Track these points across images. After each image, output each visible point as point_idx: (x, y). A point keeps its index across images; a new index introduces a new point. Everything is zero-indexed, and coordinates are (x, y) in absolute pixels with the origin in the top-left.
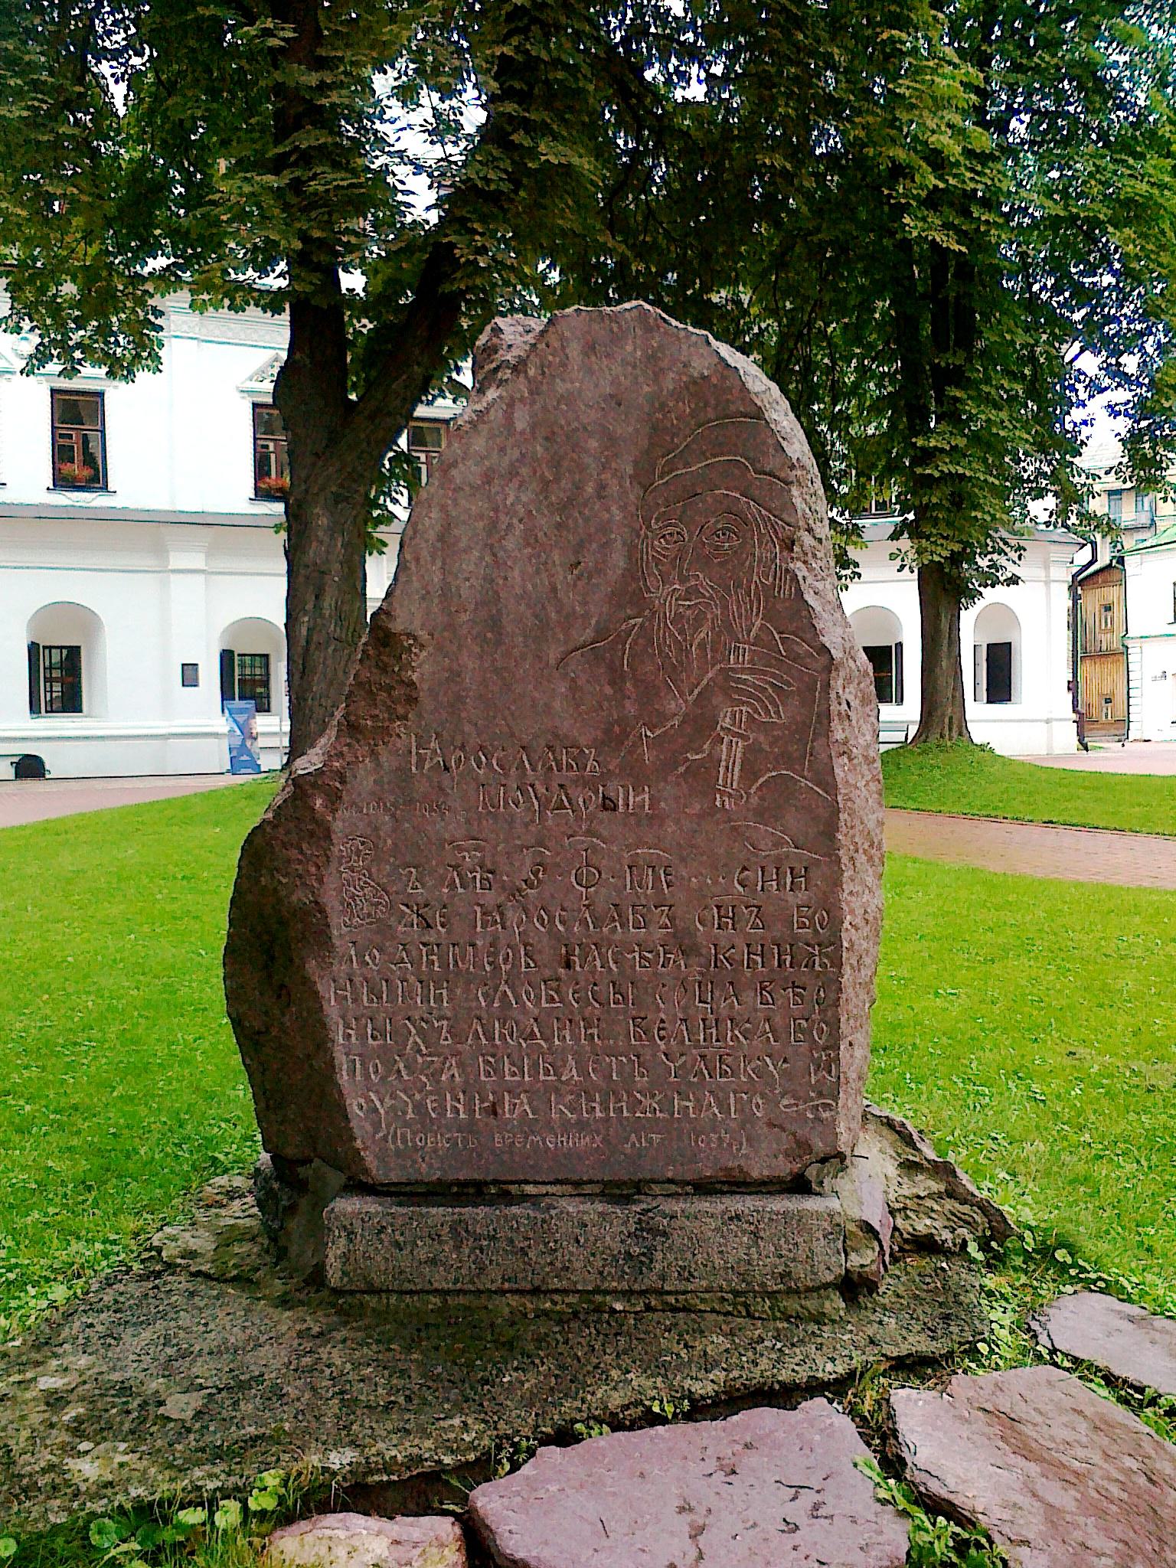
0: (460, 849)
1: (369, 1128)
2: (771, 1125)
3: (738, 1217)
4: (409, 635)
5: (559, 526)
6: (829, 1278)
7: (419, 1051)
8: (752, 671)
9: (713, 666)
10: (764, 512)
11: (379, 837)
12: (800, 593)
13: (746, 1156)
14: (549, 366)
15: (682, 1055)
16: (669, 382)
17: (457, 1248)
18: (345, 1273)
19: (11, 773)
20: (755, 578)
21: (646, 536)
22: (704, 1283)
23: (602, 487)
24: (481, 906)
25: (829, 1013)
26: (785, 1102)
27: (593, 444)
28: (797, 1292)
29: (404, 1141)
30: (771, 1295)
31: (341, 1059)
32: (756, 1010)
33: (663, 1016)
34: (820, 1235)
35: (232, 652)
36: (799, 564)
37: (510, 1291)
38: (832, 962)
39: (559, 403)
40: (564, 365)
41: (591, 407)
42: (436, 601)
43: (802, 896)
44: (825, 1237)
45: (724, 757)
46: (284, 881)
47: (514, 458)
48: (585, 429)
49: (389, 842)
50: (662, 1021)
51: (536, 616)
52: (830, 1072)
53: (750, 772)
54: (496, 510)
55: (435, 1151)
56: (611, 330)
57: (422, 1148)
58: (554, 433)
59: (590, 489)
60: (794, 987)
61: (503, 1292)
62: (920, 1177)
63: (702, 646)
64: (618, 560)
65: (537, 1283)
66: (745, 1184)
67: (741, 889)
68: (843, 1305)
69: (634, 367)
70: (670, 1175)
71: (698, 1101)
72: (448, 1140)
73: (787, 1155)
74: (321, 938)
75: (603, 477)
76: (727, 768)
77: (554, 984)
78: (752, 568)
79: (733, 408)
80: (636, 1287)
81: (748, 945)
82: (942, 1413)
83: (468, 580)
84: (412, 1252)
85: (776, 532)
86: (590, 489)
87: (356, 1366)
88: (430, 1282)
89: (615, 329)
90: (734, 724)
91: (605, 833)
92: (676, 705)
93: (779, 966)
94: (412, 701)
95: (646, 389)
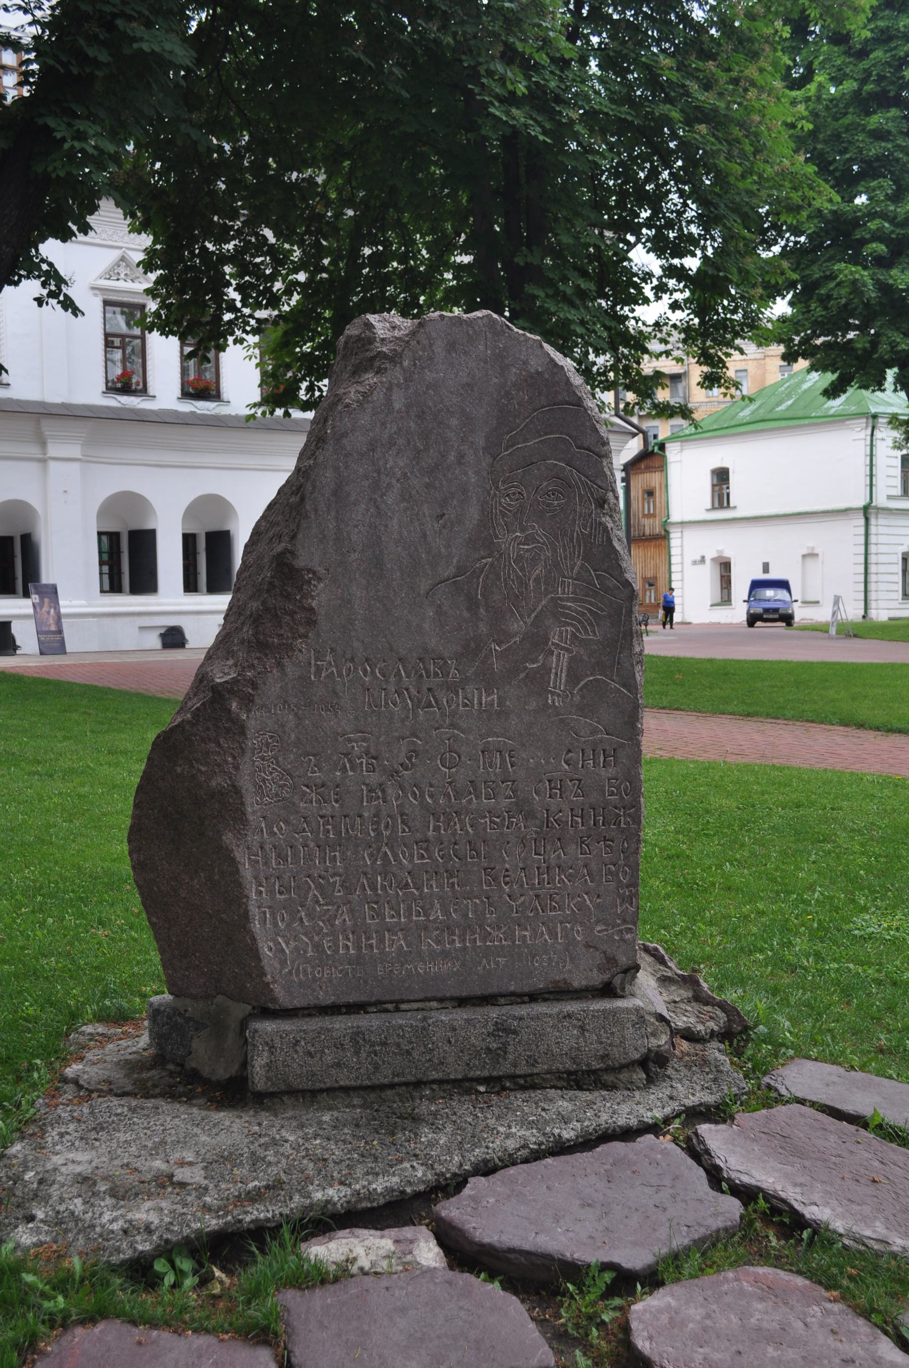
0: (350, 740)
1: (277, 966)
2: (588, 946)
4: (309, 571)
5: (428, 486)
6: (636, 1056)
7: (317, 902)
8: (574, 600)
10: (583, 478)
11: (284, 732)
12: (610, 541)
13: (570, 971)
17: (357, 1053)
18: (268, 1079)
21: (495, 495)
22: (545, 1067)
23: (461, 456)
24: (367, 785)
27: (454, 422)
31: (254, 911)
32: (577, 859)
33: (507, 866)
38: (633, 820)
40: (431, 358)
42: (331, 543)
43: (612, 771)
44: (633, 1026)
46: (203, 769)
49: (293, 736)
50: (507, 870)
51: (411, 556)
53: (573, 678)
54: (379, 472)
55: (330, 981)
58: (423, 412)
59: (452, 457)
63: (537, 580)
64: (473, 513)
65: (419, 1076)
66: (569, 992)
69: (486, 362)
70: (512, 988)
71: (534, 931)
72: (342, 971)
73: (599, 969)
74: (239, 817)
76: (556, 674)
77: (424, 845)
78: (574, 520)
79: (560, 397)
80: (495, 1073)
81: (572, 810)
83: (356, 526)
85: (592, 494)
86: (452, 457)
91: (464, 725)
92: (517, 626)
94: (311, 623)
95: (495, 380)
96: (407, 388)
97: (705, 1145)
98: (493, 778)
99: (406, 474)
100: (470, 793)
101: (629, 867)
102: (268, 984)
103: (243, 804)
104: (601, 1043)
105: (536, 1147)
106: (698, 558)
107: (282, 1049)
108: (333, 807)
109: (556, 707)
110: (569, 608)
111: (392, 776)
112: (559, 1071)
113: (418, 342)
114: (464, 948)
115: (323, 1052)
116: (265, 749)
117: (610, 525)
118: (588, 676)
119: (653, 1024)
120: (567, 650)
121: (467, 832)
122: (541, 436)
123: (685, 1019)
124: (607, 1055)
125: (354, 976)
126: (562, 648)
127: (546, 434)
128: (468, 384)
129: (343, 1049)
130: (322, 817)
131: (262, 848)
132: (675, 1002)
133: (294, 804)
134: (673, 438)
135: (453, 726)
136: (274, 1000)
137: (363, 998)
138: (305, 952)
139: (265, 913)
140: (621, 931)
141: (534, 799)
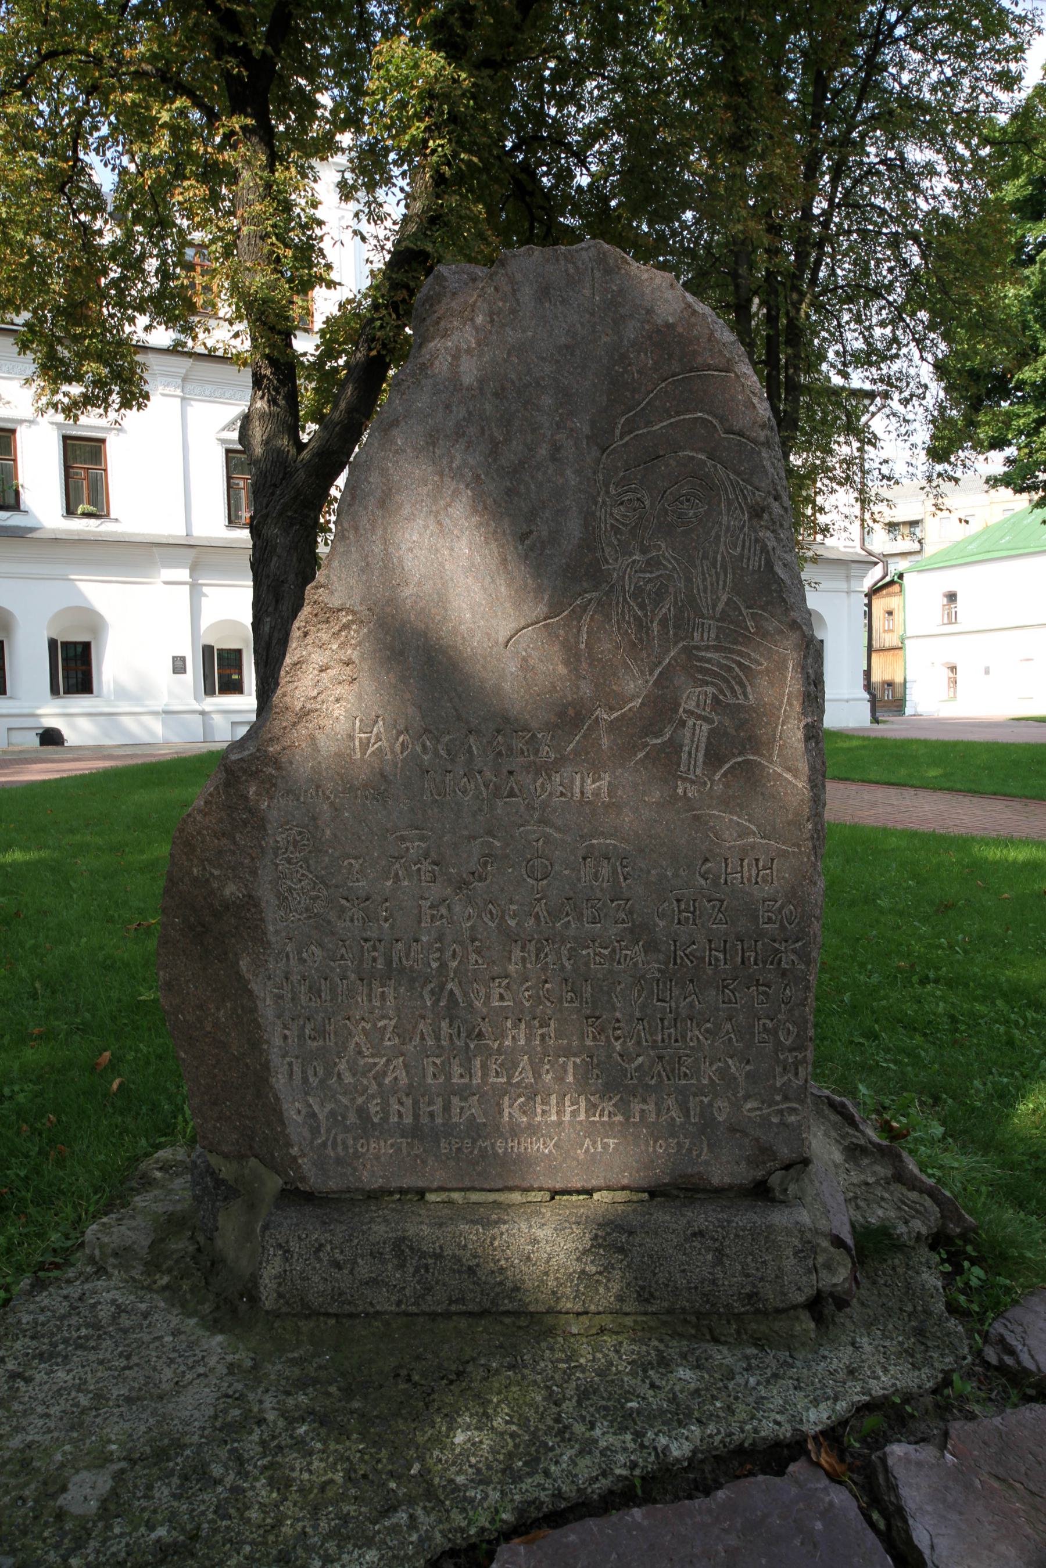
0: (403, 839)
1: (306, 1133)
3: (701, 1234)
6: (801, 1299)
7: (360, 1053)
8: (717, 649)
9: (676, 643)
10: (732, 476)
11: (317, 827)
12: (770, 565)
13: (707, 1163)
14: (498, 314)
15: (638, 1056)
16: (631, 331)
18: (280, 1295)
19: (37, 740)
20: (722, 548)
21: (604, 503)
22: (666, 1304)
23: (556, 449)
25: (796, 1013)
26: (749, 1106)
27: (547, 401)
28: (765, 1313)
29: (346, 1148)
30: (738, 1317)
31: (275, 1060)
32: (717, 1009)
33: (618, 1015)
34: (789, 1252)
35: (212, 647)
36: (769, 534)
37: (456, 1313)
39: (509, 354)
41: (543, 359)
42: (376, 573)
44: (795, 1254)
45: (687, 741)
46: (216, 873)
47: (461, 416)
48: (538, 384)
49: (328, 832)
50: (618, 1021)
52: (796, 1074)
55: (377, 1157)
56: (566, 271)
57: (363, 1154)
58: (503, 389)
60: (758, 984)
61: (447, 1315)
62: (865, 1162)
63: (664, 622)
64: (574, 527)
65: (487, 1305)
66: (705, 1191)
67: (703, 882)
68: (812, 1325)
69: (592, 314)
72: (392, 1145)
75: (557, 437)
76: (690, 753)
78: (718, 537)
79: (700, 360)
81: (710, 941)
82: (951, 1484)
83: (411, 550)
84: (351, 1272)
85: (745, 498)
86: (543, 451)
87: (291, 1420)
88: (371, 1304)
89: (571, 271)
90: (698, 706)
93: (743, 963)
95: (605, 339)
96: (481, 355)
97: (898, 1496)
98: (599, 895)
99: (478, 476)
100: (567, 915)
101: (794, 1023)
102: (295, 1159)
103: (262, 920)
104: (747, 1276)
105: (624, 1472)
106: (946, 673)
107: (301, 1255)
108: (380, 928)
109: (689, 799)
110: (709, 661)
111: (460, 888)
112: (684, 1310)
113: (496, 289)
114: (560, 1123)
115: (355, 1263)
116: (291, 848)
117: (771, 544)
118: (734, 756)
119: (824, 1250)
120: (706, 719)
121: (563, 968)
122: (671, 417)
123: (880, 1212)
124: (757, 1294)
125: (409, 1154)
126: (699, 717)
127: (678, 414)
128: (567, 347)
129: (384, 1262)
130: (366, 940)
131: (287, 979)
132: (867, 1184)
133: (329, 922)
134: (910, 571)
135: (543, 821)
136: (303, 1179)
137: (421, 1184)
138: (344, 1118)
139: (290, 1064)
140: (781, 1112)
141: (656, 925)
